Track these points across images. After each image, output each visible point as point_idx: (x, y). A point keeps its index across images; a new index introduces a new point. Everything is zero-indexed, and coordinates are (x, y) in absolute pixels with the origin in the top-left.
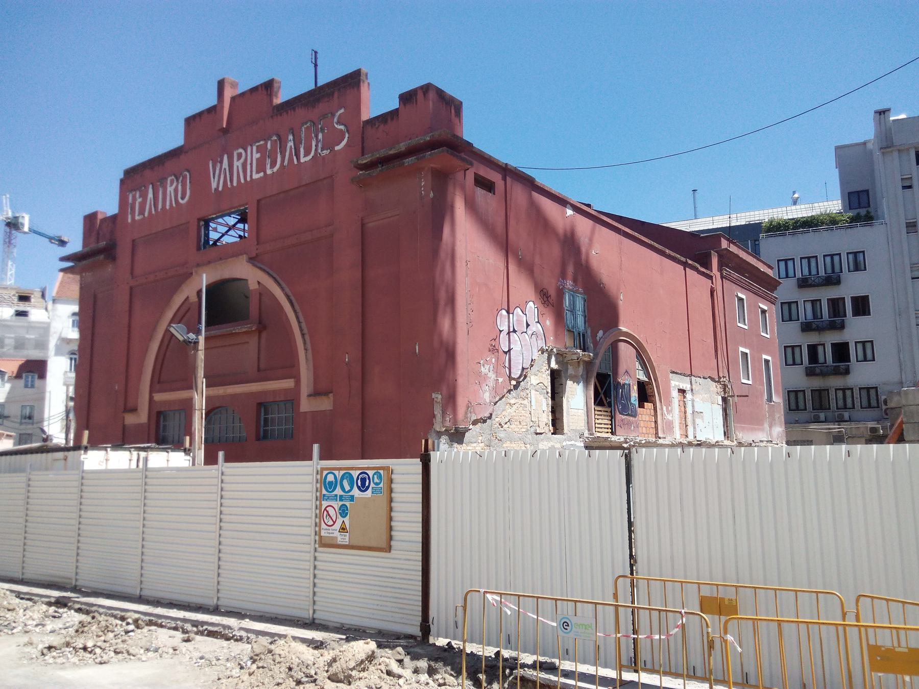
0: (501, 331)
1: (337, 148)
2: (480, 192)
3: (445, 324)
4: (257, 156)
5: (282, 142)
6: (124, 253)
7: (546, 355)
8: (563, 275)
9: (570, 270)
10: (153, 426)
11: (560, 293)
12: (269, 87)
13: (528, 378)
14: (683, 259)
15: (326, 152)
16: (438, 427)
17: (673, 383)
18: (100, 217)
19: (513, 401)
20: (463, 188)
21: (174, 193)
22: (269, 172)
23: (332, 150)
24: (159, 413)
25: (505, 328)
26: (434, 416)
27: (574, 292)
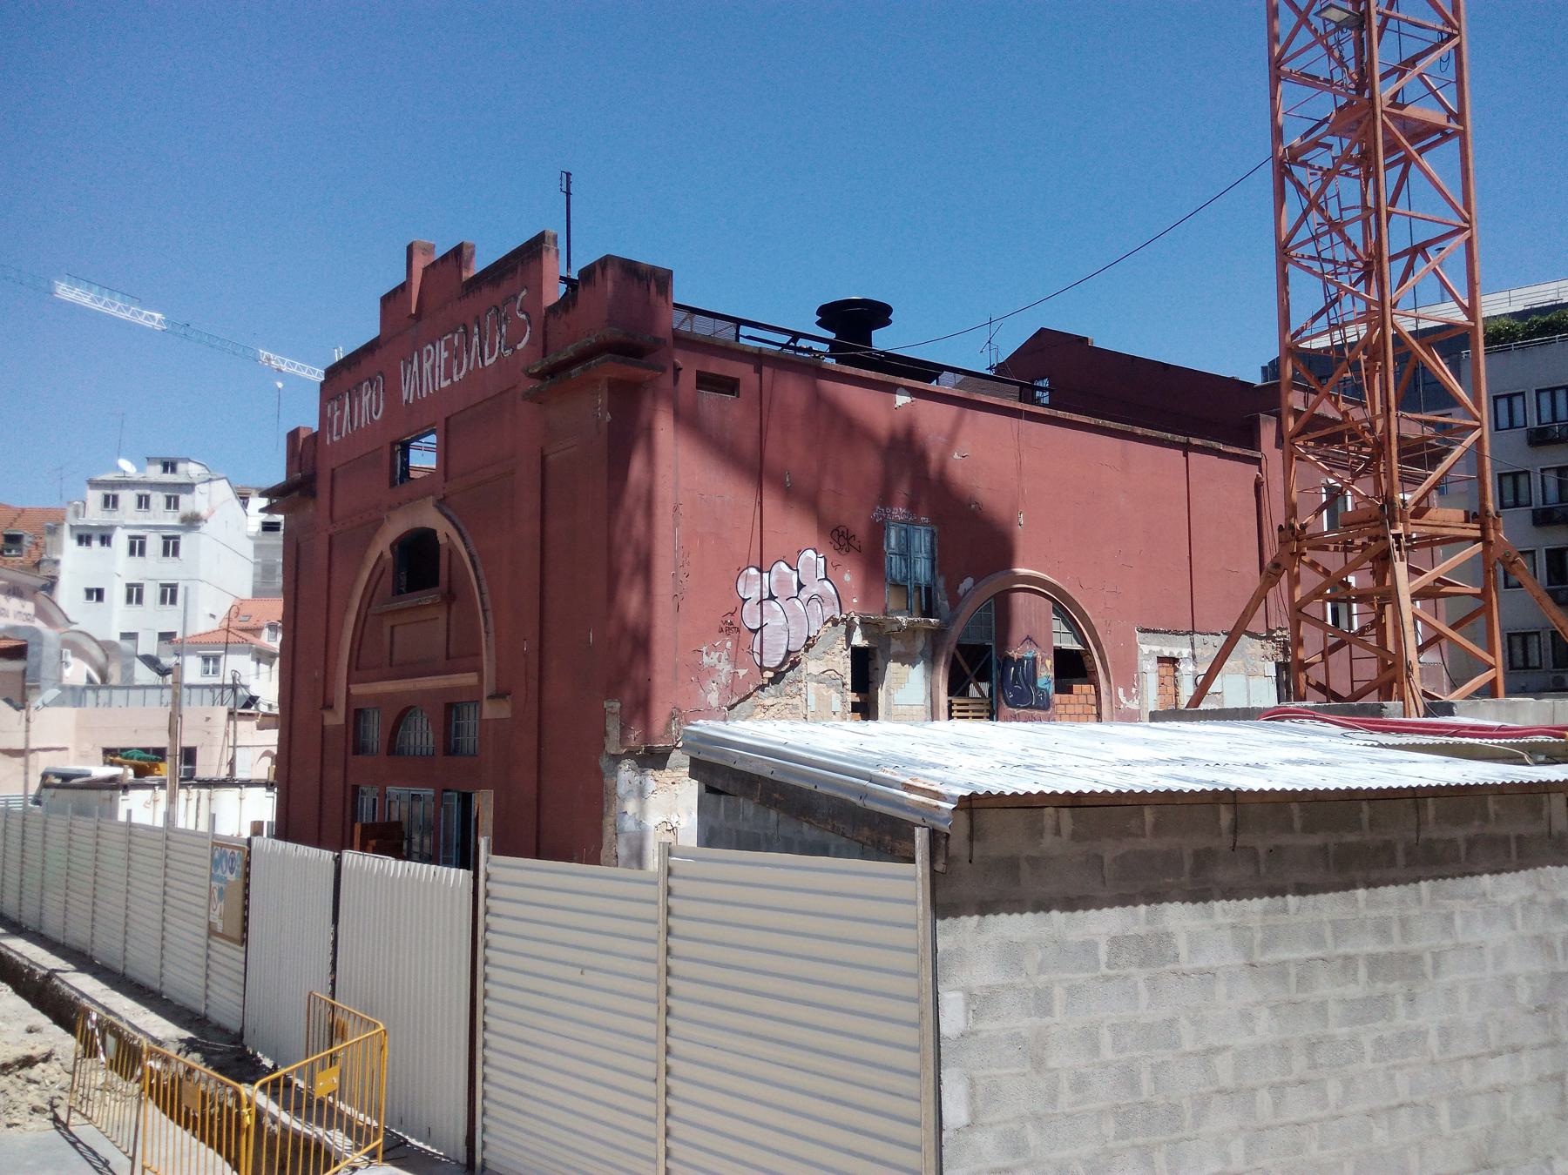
0: (745, 600)
1: (520, 346)
2: (709, 398)
3: (632, 601)
4: (445, 355)
5: (468, 334)
6: (323, 486)
7: (842, 627)
8: (886, 499)
9: (902, 491)
10: (351, 729)
11: (878, 531)
12: (458, 255)
13: (802, 666)
14: (1182, 439)
15: (508, 352)
16: (613, 747)
17: (1145, 649)
18: (303, 435)
19: (768, 702)
20: (673, 400)
21: (369, 404)
22: (456, 379)
23: (514, 349)
24: (358, 712)
25: (754, 594)
26: (606, 734)
27: (910, 524)
